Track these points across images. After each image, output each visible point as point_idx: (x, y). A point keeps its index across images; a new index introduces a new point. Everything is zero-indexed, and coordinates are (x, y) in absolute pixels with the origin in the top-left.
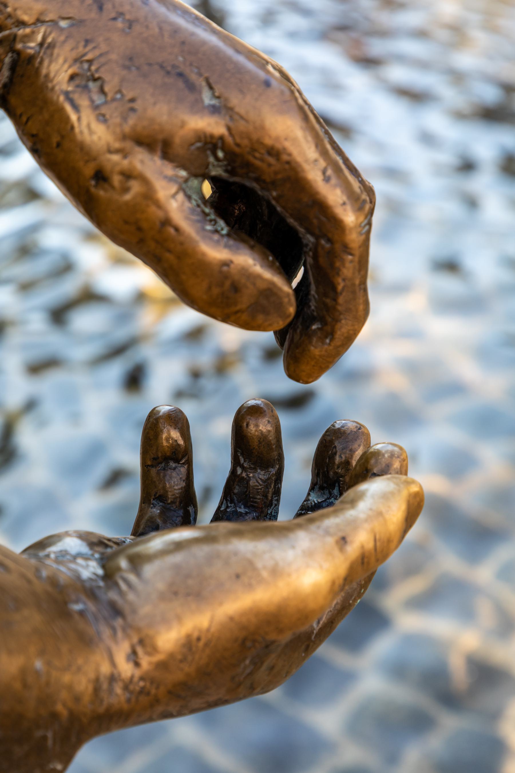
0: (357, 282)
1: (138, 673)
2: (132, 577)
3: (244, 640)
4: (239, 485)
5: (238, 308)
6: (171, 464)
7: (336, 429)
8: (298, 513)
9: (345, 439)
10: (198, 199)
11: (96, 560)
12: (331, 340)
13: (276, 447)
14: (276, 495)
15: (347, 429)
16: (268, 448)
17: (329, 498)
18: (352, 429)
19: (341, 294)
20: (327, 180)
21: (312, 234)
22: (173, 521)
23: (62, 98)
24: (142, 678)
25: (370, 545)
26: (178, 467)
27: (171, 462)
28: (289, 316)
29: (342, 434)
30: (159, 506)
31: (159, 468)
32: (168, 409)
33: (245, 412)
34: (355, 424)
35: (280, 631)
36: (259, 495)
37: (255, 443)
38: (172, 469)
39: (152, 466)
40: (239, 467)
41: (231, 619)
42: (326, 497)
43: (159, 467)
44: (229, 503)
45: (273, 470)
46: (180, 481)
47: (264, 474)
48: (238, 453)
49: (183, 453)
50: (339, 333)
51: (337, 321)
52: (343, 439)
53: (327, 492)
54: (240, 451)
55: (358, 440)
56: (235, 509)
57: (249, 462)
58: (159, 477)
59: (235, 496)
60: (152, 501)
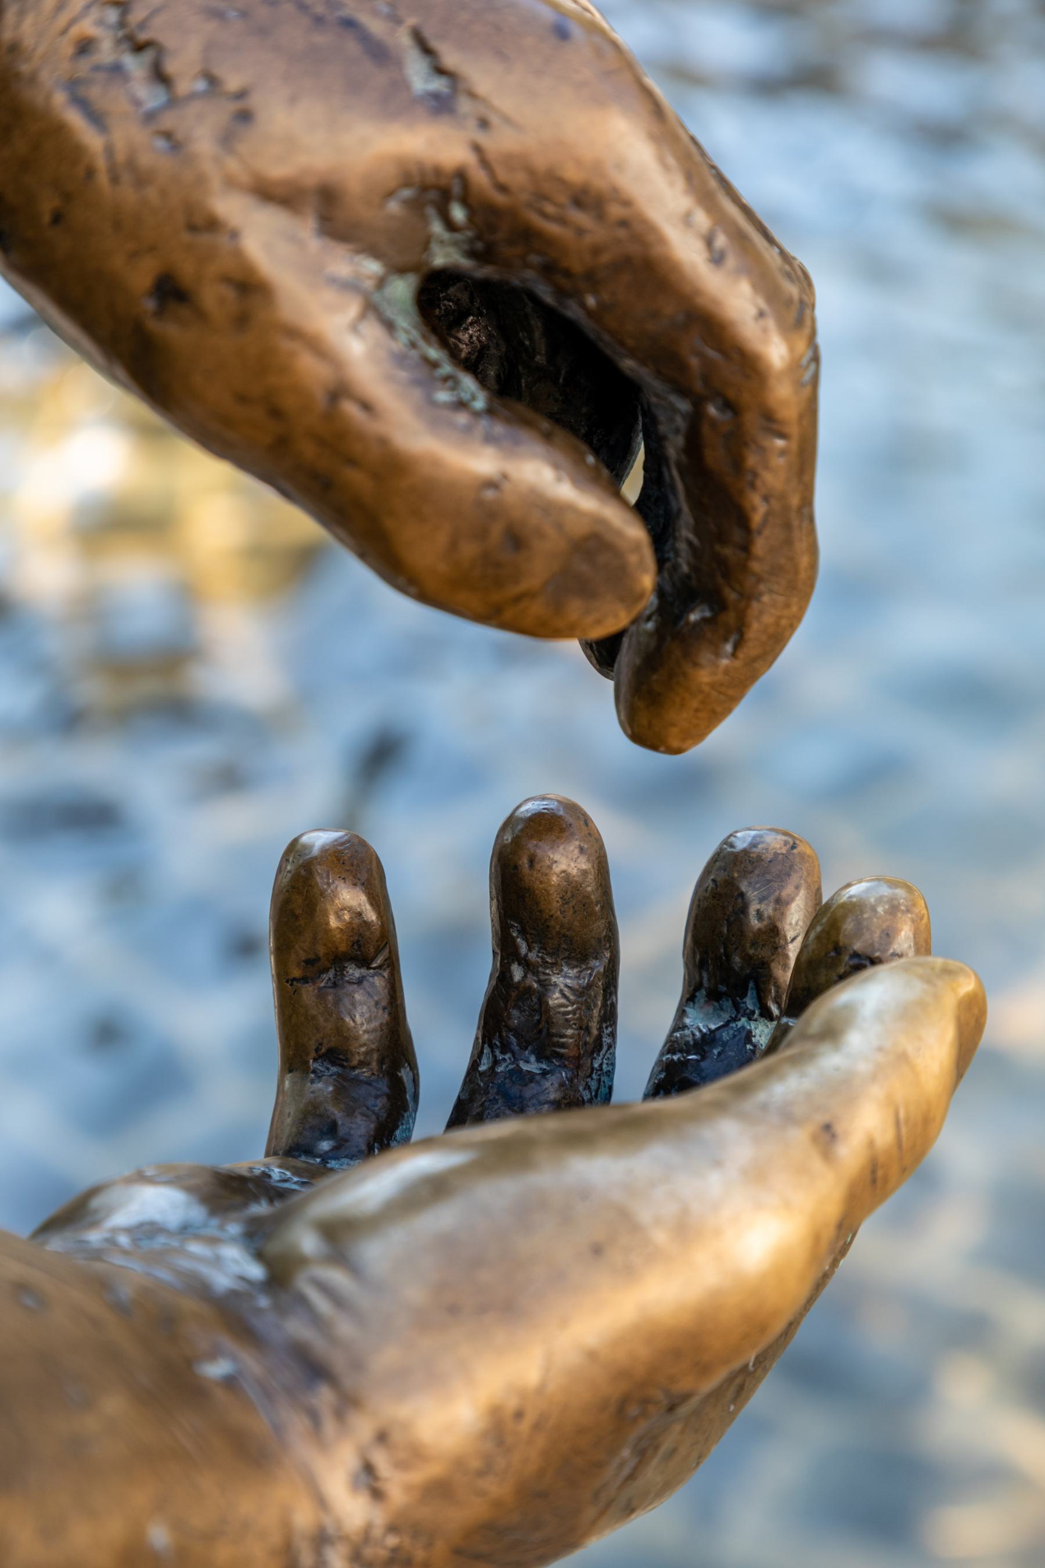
0: (795, 501)
1: (379, 1517)
2: (337, 1277)
3: (624, 1402)
4: (519, 1008)
5: (524, 586)
6: (351, 971)
7: (739, 853)
8: (662, 1061)
9: (763, 875)
10: (409, 328)
11: (233, 1240)
12: (737, 647)
13: (602, 908)
14: (608, 1024)
15: (764, 851)
16: (585, 913)
17: (735, 1019)
18: (775, 848)
19: (759, 532)
20: (717, 259)
21: (684, 392)
22: (368, 1109)
23: (60, 98)
24: (392, 1528)
25: (885, 1138)
26: (368, 978)
27: (349, 967)
28: (641, 596)
29: (753, 862)
30: (331, 1075)
31: (322, 984)
32: (332, 840)
33: (522, 830)
34: (781, 838)
35: (704, 1369)
36: (570, 1027)
37: (555, 904)
38: (354, 983)
39: (305, 980)
40: (516, 963)
41: (592, 1355)
42: (726, 1016)
43: (322, 981)
44: (497, 1052)
45: (597, 964)
46: (375, 1010)
47: (579, 976)
48: (511, 930)
49: (377, 941)
50: (755, 626)
51: (748, 597)
52: (758, 876)
53: (728, 1004)
54: (516, 925)
55: (792, 873)
56: (514, 1066)
57: (542, 951)
58: (323, 1005)
59: (510, 1033)
60: (313, 1065)
